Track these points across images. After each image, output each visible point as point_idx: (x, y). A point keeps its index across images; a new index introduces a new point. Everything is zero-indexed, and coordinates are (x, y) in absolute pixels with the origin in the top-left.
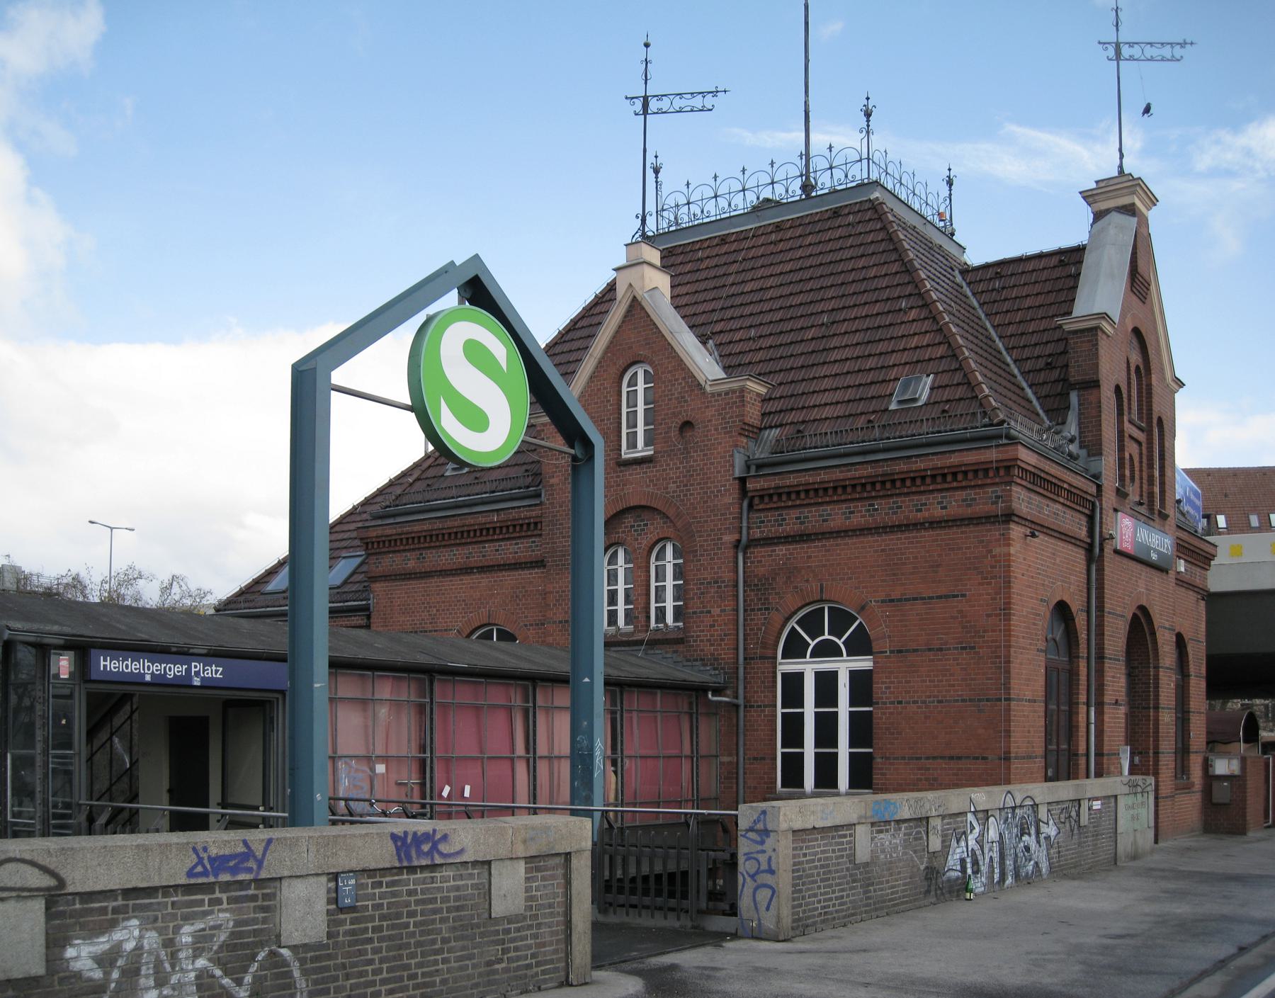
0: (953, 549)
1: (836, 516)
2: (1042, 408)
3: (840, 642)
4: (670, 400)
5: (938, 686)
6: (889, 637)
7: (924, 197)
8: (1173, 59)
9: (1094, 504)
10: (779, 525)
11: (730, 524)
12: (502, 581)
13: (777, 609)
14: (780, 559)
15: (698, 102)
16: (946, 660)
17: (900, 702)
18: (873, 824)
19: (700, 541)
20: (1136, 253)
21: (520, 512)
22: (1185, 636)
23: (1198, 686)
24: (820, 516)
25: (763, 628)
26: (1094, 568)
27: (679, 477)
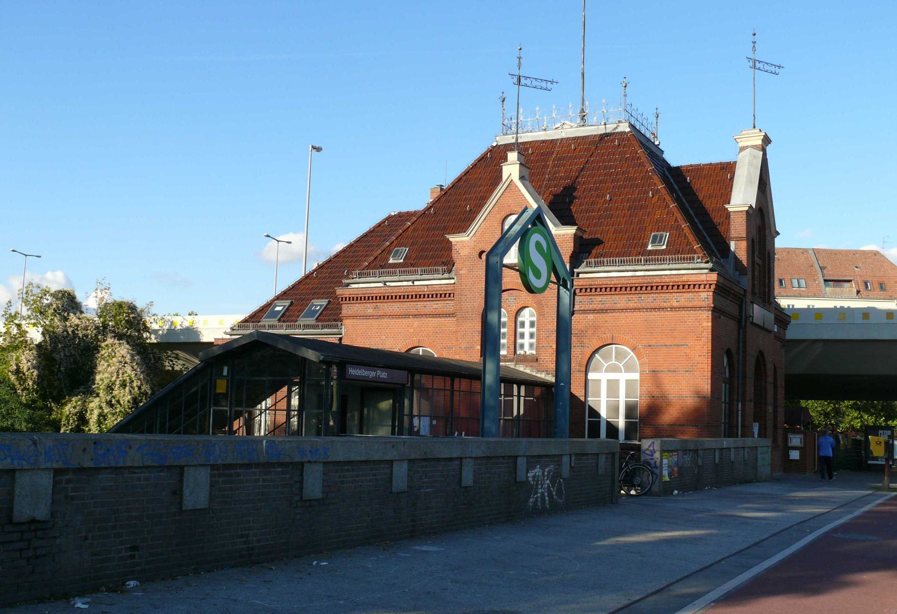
0: (682, 322)
1: (621, 300)
2: (716, 248)
3: (621, 365)
6: (648, 364)
7: (646, 126)
8: (775, 73)
10: (590, 304)
12: (427, 323)
13: (588, 347)
14: (590, 322)
15: (544, 84)
19: (547, 310)
23: (781, 392)
24: (612, 301)
25: (580, 356)
26: (741, 331)
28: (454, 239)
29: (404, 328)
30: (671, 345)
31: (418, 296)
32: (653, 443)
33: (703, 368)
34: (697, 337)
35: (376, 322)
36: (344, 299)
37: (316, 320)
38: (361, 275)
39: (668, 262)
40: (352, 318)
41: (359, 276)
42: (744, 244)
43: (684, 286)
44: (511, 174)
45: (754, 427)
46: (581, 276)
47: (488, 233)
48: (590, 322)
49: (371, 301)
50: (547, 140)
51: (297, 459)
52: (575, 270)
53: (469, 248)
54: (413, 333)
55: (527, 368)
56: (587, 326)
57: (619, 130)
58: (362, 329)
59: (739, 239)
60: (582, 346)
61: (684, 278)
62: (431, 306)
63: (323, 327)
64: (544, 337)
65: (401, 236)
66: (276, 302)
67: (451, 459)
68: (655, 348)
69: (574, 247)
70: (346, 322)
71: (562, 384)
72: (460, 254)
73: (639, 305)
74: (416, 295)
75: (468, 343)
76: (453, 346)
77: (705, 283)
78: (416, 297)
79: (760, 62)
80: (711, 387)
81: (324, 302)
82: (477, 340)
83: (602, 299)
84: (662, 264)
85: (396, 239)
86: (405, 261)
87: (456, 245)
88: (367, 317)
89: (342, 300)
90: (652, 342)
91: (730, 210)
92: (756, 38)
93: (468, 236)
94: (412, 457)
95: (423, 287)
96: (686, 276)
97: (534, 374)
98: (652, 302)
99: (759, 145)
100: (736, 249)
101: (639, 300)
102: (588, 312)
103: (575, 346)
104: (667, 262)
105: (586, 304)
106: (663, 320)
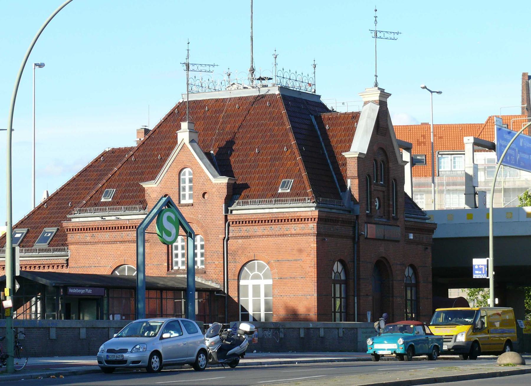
1: (259, 230)
3: (261, 274)
4: (199, 183)
5: (294, 290)
6: (277, 273)
8: (394, 39)
9: (355, 222)
11: (222, 231)
12: (130, 247)
15: (207, 68)
16: (296, 281)
17: (281, 296)
18: (263, 328)
19: (211, 237)
20: (379, 121)
21: (139, 221)
22: (415, 265)
24: (254, 230)
25: (234, 269)
27: (202, 213)
28: (146, 185)
29: (113, 251)
30: (292, 260)
31: (122, 228)
32: (236, 324)
33: (312, 276)
34: (308, 254)
35: (93, 247)
36: (69, 230)
37: (48, 245)
38: (80, 211)
39: (289, 202)
40: (75, 244)
41: (79, 212)
42: (356, 181)
43: (298, 219)
44: (183, 139)
45: (367, 315)
46: (234, 212)
47: (169, 182)
48: (240, 244)
49: (89, 231)
50: (220, 99)
51: (48, 326)
52: (229, 208)
53: (157, 193)
54: (120, 254)
55: (199, 278)
56: (238, 248)
57: (270, 93)
58: (83, 252)
59: (353, 178)
60: (235, 262)
61: (298, 214)
62: (132, 235)
63: (54, 251)
64: (209, 256)
65: (110, 179)
66: (15, 230)
67: (104, 328)
68: (282, 262)
69: (227, 192)
70: (71, 247)
71: (191, 293)
72: (151, 196)
73: (271, 233)
74: (121, 227)
75: (159, 261)
76: (149, 263)
77: (311, 217)
78: (121, 228)
79: (380, 32)
80: (317, 288)
81: (54, 230)
82: (164, 259)
83: (247, 228)
84: (286, 203)
85: (107, 181)
86: (113, 200)
87: (148, 190)
88: (86, 243)
89: (67, 231)
90: (280, 259)
91: (346, 156)
92: (377, 14)
93: (155, 184)
94: (87, 327)
95: (126, 221)
96: (299, 212)
97: (203, 282)
98: (279, 231)
99: (377, 100)
100: (351, 185)
101: (270, 229)
102: (238, 238)
103: (230, 262)
104: (288, 202)
105: (237, 232)
106: (286, 243)
